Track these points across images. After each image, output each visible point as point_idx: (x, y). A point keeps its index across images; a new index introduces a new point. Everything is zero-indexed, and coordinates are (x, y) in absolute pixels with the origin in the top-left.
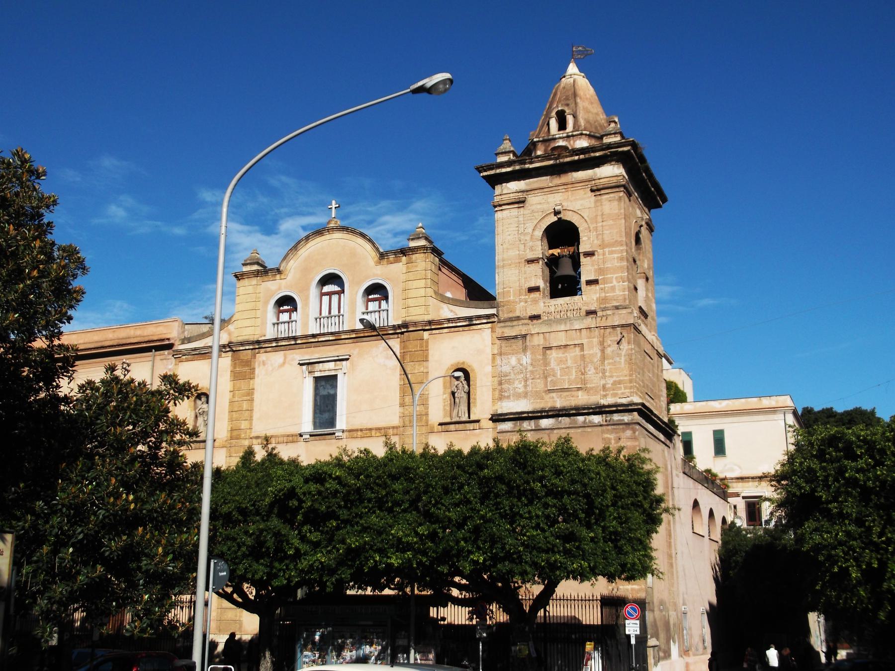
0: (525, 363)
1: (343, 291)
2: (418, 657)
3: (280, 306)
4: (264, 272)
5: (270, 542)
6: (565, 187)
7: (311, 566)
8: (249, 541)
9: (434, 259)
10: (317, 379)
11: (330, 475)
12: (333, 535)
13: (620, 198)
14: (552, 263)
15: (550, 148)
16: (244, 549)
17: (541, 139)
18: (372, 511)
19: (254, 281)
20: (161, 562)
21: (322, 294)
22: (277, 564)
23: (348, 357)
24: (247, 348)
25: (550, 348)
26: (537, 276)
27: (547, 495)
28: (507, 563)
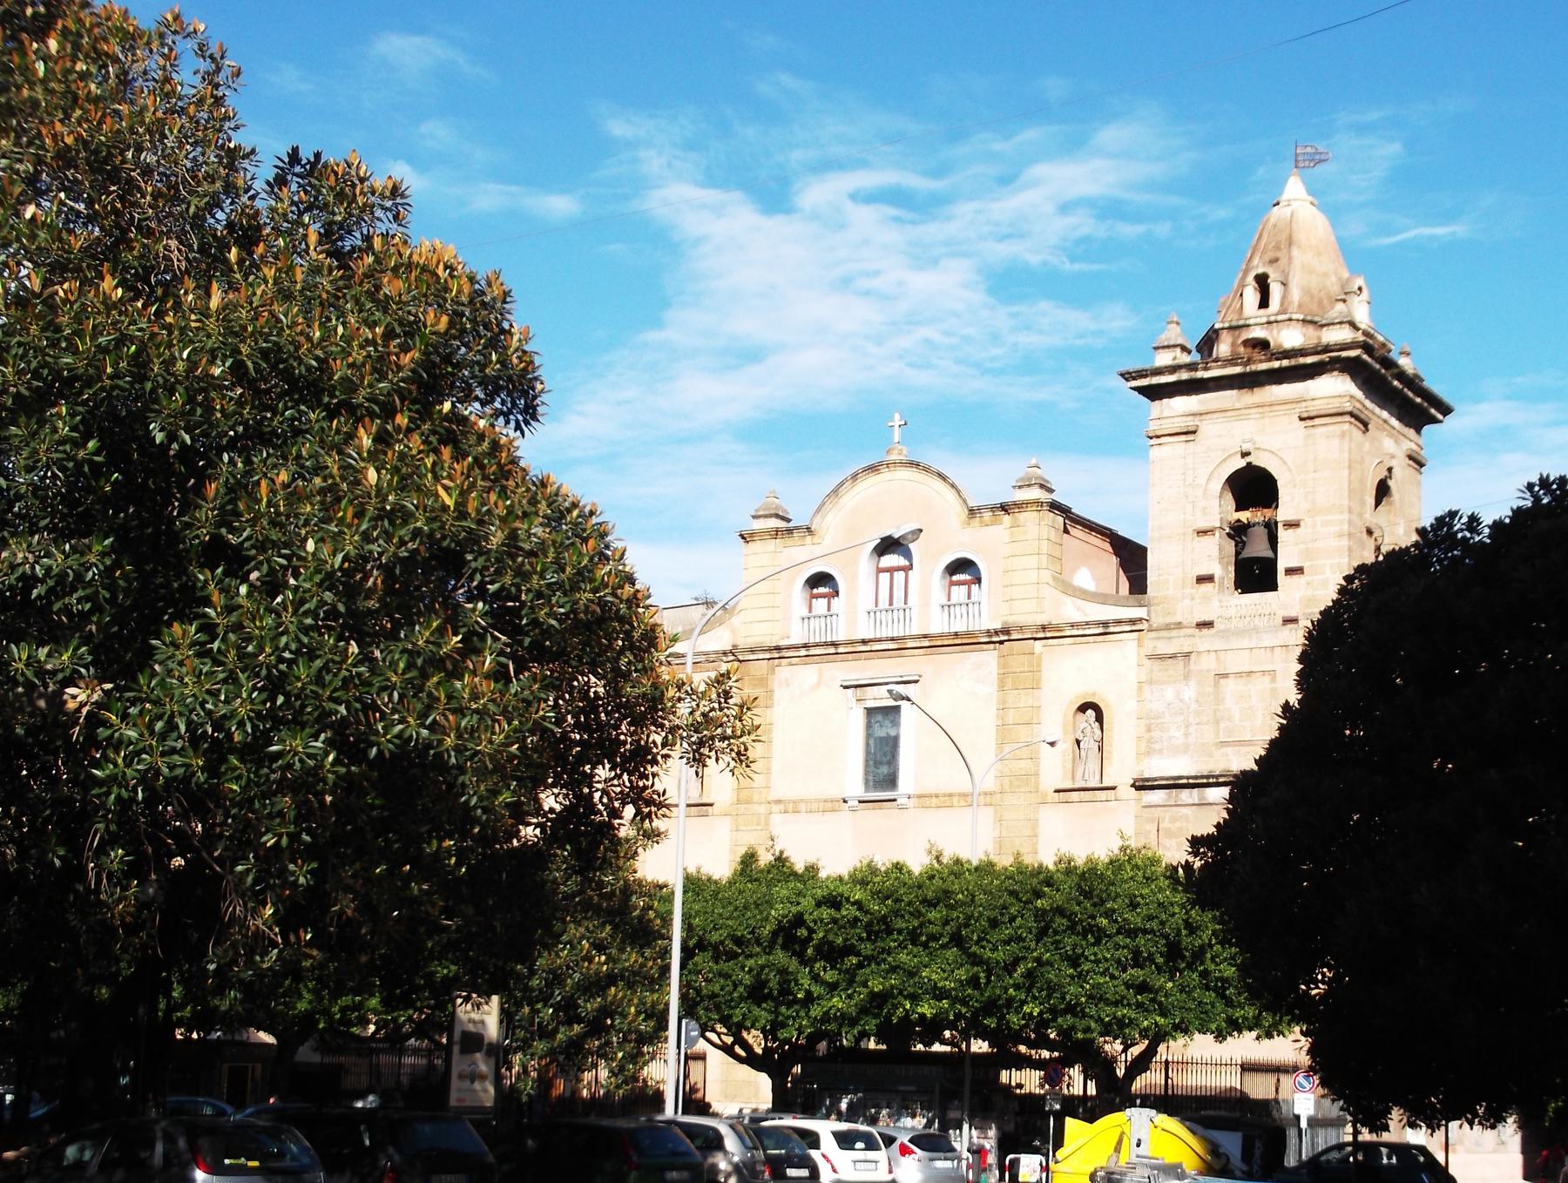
0: (1187, 698)
1: (911, 567)
2: (974, 1132)
3: (812, 588)
4: (787, 530)
5: (774, 981)
6: (1260, 410)
7: (827, 1013)
8: (748, 980)
9: (1054, 521)
10: (870, 712)
11: (848, 899)
12: (854, 976)
13: (1343, 434)
14: (1238, 532)
15: (1240, 341)
16: (741, 989)
17: (1227, 325)
18: (902, 946)
19: (771, 545)
20: (633, 1021)
21: (880, 571)
22: (783, 1009)
23: (916, 678)
24: (761, 656)
25: (1225, 676)
26: (1216, 557)
27: (1119, 932)
28: (1069, 1017)
